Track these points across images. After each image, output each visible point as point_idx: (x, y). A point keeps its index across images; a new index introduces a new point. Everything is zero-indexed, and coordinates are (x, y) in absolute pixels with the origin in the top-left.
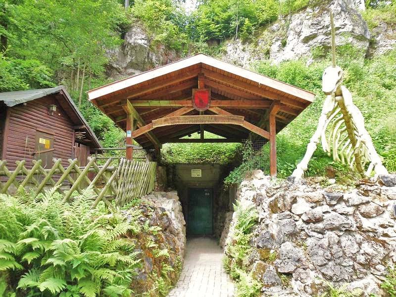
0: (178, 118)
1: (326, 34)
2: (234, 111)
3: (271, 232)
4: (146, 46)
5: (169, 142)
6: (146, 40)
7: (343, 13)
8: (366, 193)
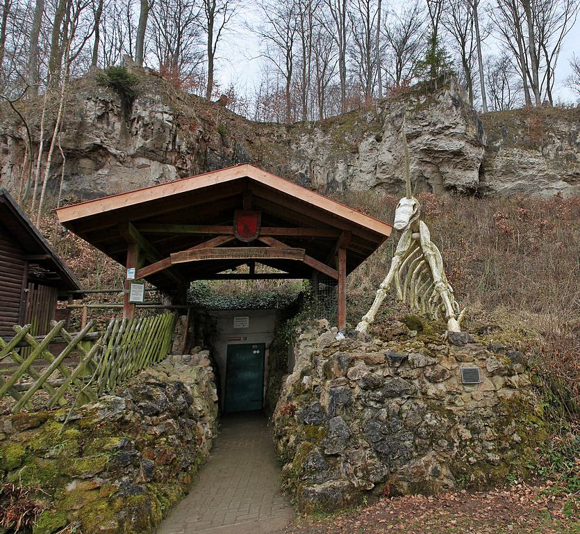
0: (211, 251)
1: (433, 133)
2: (291, 242)
3: (322, 404)
4: (170, 124)
5: (201, 278)
6: (170, 115)
7: (454, 108)
8: (433, 353)
